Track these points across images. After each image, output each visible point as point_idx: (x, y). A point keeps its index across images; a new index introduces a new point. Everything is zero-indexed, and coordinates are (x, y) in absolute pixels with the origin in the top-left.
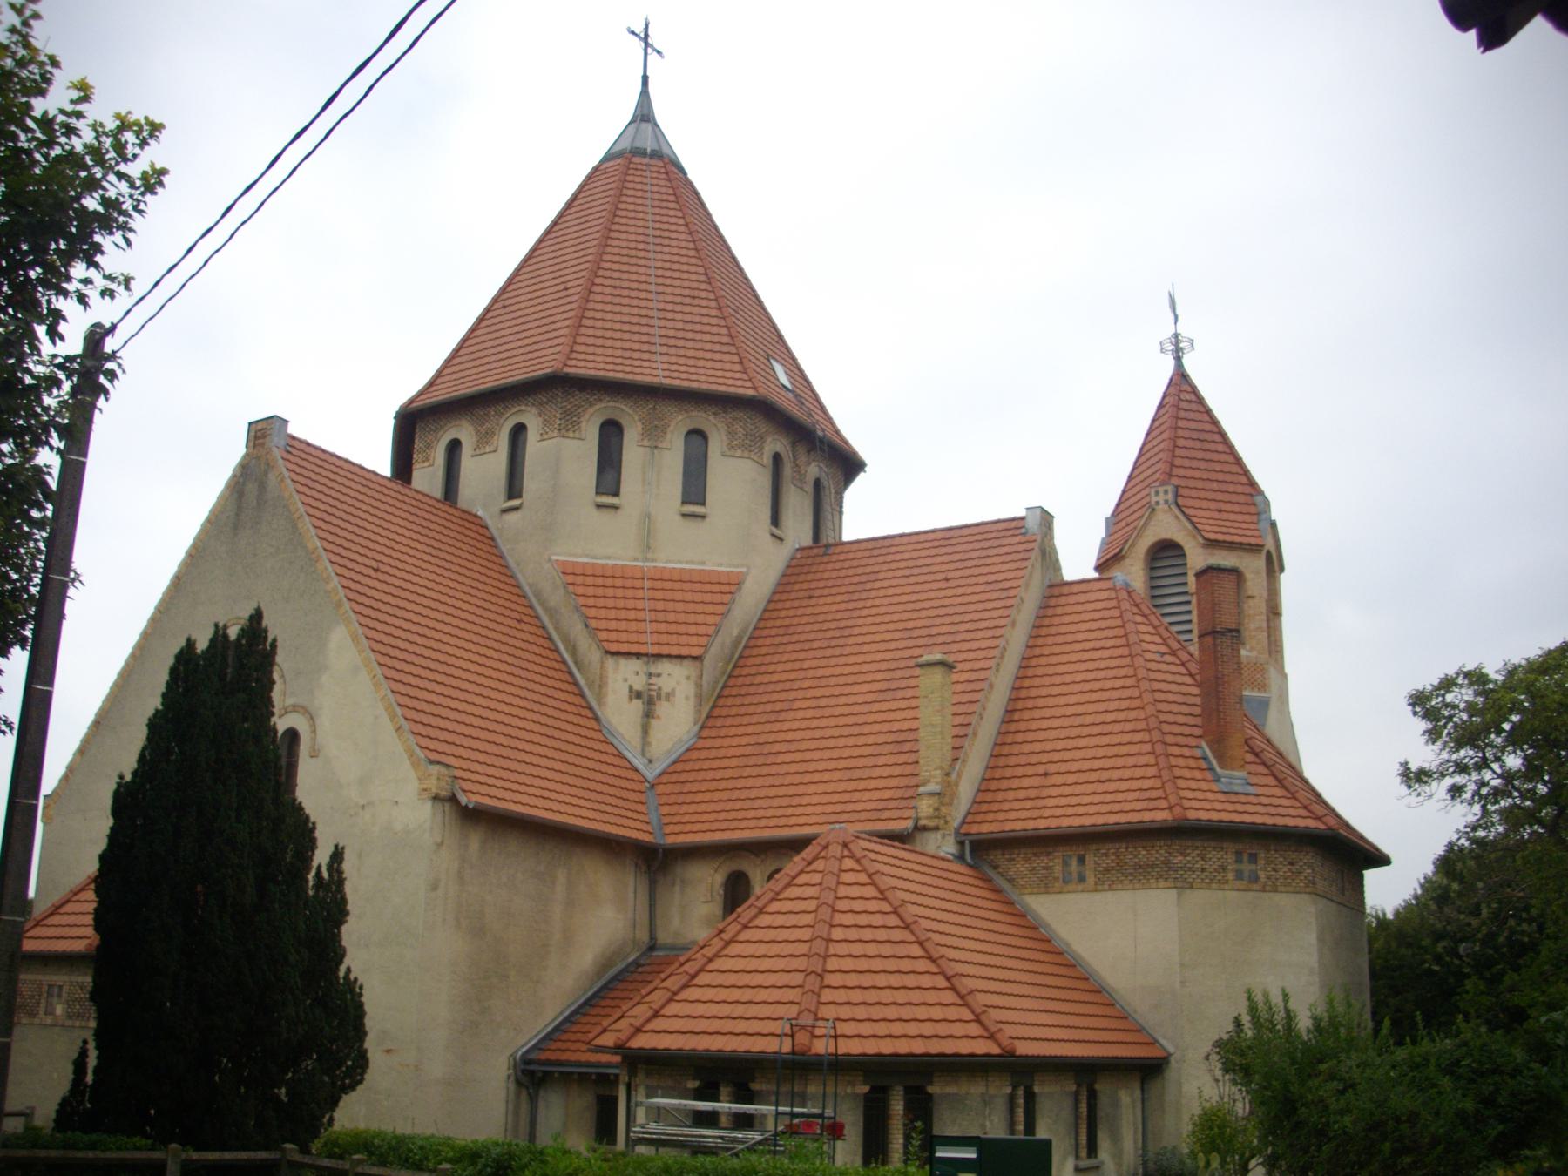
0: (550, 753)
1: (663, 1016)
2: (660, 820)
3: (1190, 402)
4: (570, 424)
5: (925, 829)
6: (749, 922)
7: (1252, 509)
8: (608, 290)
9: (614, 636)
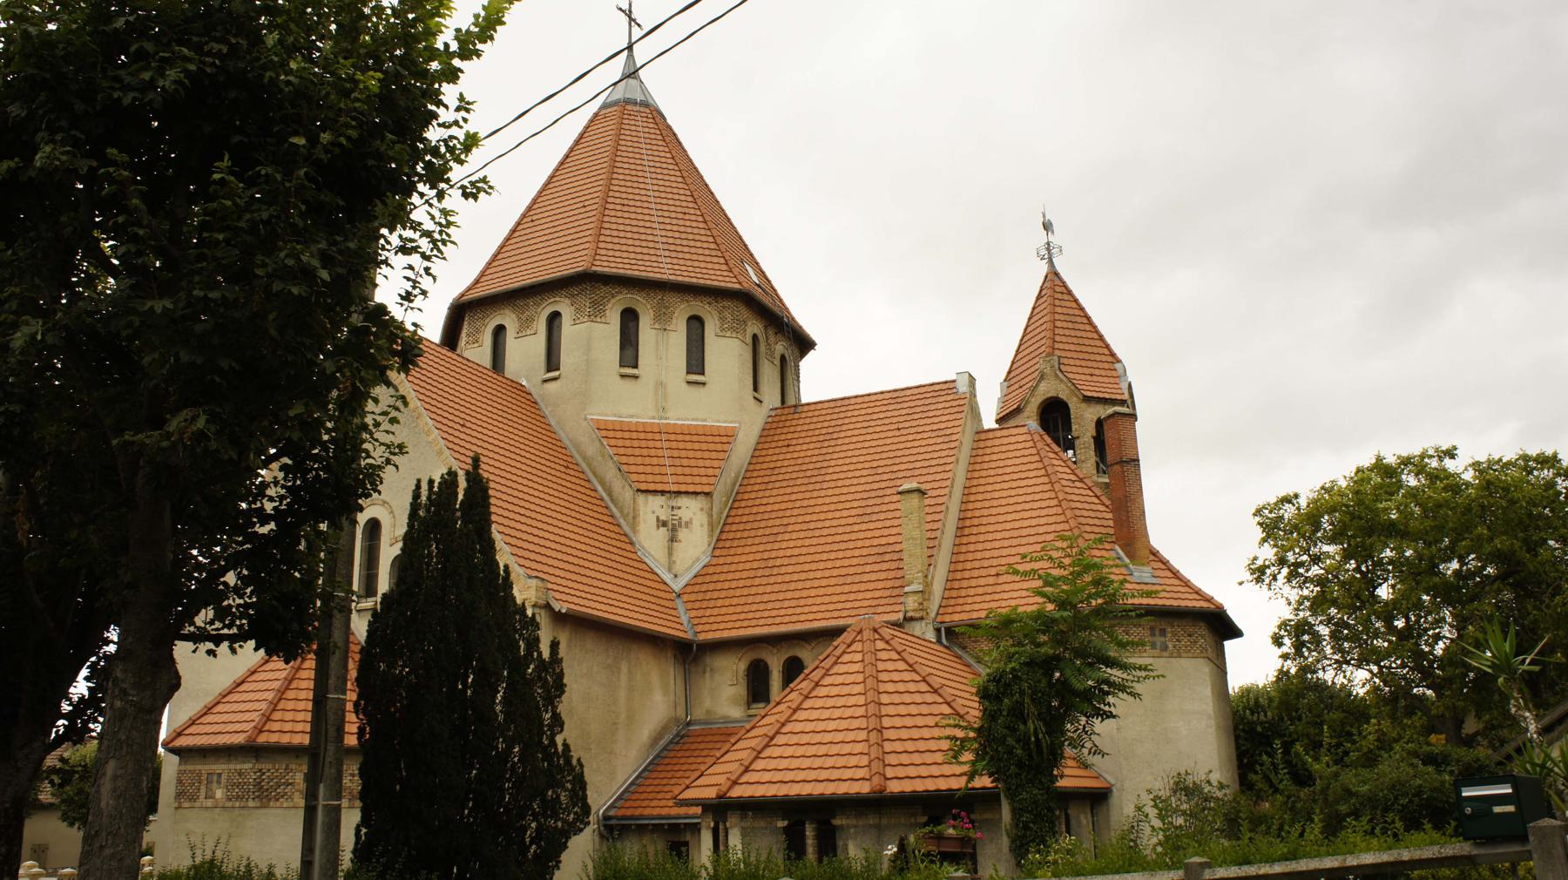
0: (607, 570)
1: (753, 770)
2: (689, 622)
3: (1062, 293)
4: (597, 312)
5: (912, 619)
6: (809, 693)
7: (1114, 373)
8: (618, 207)
9: (642, 478)
